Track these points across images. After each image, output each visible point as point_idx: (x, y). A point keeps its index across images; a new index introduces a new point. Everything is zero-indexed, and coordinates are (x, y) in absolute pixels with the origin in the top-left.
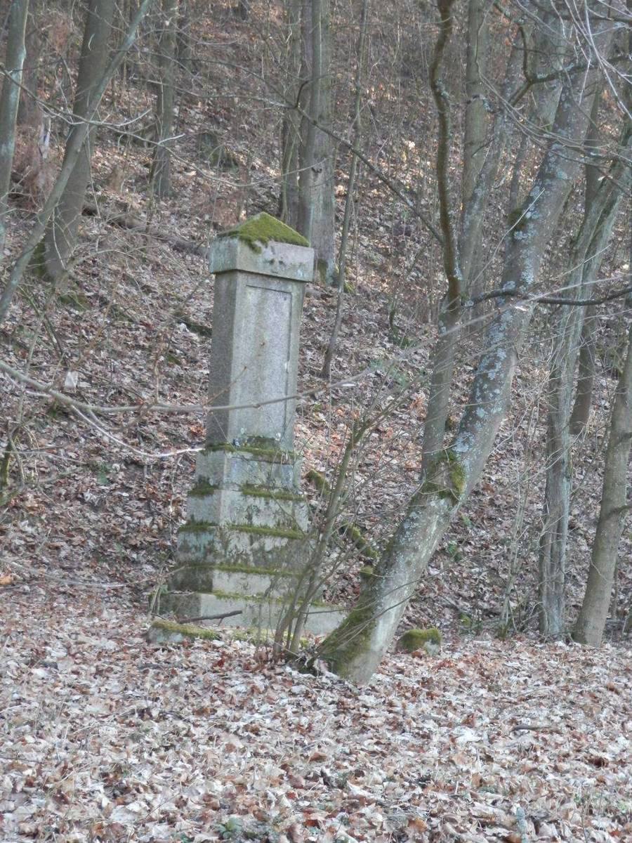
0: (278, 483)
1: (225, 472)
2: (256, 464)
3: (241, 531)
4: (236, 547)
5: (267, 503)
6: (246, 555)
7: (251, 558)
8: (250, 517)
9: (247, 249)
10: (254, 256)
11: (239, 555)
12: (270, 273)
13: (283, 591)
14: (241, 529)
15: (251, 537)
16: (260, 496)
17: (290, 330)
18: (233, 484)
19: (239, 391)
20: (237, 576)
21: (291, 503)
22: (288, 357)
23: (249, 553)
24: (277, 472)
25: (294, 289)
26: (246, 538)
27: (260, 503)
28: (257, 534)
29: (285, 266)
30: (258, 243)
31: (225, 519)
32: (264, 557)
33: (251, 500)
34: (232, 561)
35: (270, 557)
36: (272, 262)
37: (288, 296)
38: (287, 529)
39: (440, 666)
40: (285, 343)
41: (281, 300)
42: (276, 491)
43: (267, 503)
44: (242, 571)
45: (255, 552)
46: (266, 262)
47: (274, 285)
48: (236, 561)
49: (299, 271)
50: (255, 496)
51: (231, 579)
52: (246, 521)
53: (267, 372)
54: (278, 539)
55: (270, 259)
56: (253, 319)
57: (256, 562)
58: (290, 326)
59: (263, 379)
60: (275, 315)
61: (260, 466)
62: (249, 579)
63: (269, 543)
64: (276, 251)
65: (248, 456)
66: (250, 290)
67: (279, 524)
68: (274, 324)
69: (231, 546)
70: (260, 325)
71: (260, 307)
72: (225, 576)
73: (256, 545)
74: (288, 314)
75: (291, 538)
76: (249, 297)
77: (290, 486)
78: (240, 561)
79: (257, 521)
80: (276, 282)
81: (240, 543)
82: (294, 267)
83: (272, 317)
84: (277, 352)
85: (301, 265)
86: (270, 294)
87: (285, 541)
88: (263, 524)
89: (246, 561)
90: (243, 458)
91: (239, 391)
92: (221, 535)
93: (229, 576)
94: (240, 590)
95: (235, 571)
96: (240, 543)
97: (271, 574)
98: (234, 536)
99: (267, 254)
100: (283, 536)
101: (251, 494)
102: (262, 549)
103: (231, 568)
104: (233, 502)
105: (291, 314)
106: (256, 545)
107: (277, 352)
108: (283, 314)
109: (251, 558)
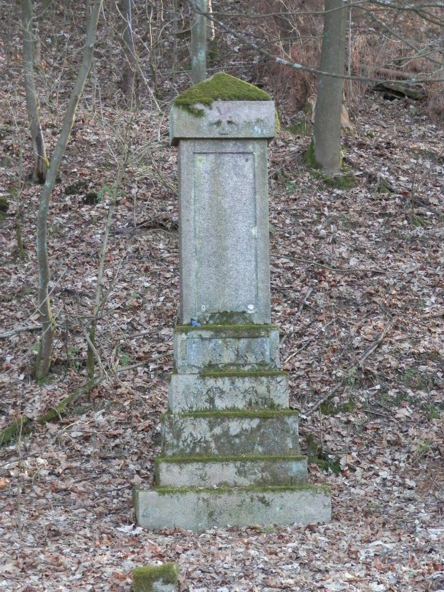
0: (251, 359)
1: (179, 355)
2: (220, 342)
3: (196, 417)
4: (191, 434)
5: (233, 383)
6: (206, 442)
7: (213, 445)
8: (211, 401)
9: (185, 114)
10: (197, 121)
11: (196, 443)
12: (218, 136)
13: (253, 477)
14: (196, 415)
15: (210, 422)
16: (222, 376)
17: (255, 193)
18: (191, 366)
19: (195, 265)
20: (191, 467)
21: (264, 379)
22: (256, 222)
23: (210, 439)
24: (249, 348)
25: (256, 149)
26: (203, 424)
27: (224, 384)
28: (216, 417)
29: (237, 125)
30: (199, 106)
31: (179, 405)
32: (230, 442)
33: (211, 382)
34: (188, 450)
35: (237, 441)
36: (218, 123)
37: (250, 156)
38: (267, 412)
39: (115, 437)
40: (251, 207)
41: (241, 161)
42: (247, 368)
43: (233, 383)
44: (198, 461)
45: (217, 438)
46: (211, 124)
47: (230, 147)
48: (194, 449)
49: (256, 128)
50: (215, 377)
51: (184, 470)
52: (207, 405)
53: (229, 242)
54: (247, 421)
55: (216, 120)
56: (206, 187)
57: (218, 448)
58: (254, 188)
59: (225, 249)
60: (235, 179)
61: (225, 342)
62: (207, 469)
63: (235, 427)
64: (223, 112)
65: (206, 334)
66: (199, 157)
67: (250, 404)
68: (235, 189)
69: (185, 435)
70: (217, 191)
71: (215, 173)
72: (175, 469)
73: (218, 430)
74: (251, 176)
75: (264, 418)
76: (199, 166)
77: (268, 361)
78: (198, 450)
79: (220, 404)
80: (231, 144)
81: (200, 430)
82: (249, 124)
83: (231, 182)
84: (240, 218)
85: (258, 121)
86: (226, 158)
87: (255, 423)
88: (229, 406)
89: (206, 449)
90: (202, 339)
91: (195, 265)
92: (171, 424)
93: (181, 468)
94: (196, 481)
95: (187, 462)
96: (200, 430)
97: (235, 460)
98: (189, 422)
99: (212, 114)
100: (252, 417)
101: (210, 376)
102: (226, 433)
103: (182, 460)
104: (188, 387)
105: (254, 176)
106: (218, 430)
107: (240, 218)
108: (245, 176)
109: (213, 445)
